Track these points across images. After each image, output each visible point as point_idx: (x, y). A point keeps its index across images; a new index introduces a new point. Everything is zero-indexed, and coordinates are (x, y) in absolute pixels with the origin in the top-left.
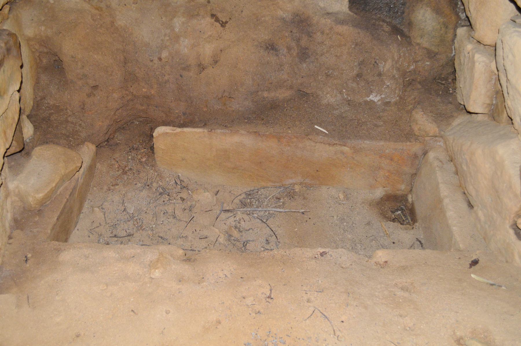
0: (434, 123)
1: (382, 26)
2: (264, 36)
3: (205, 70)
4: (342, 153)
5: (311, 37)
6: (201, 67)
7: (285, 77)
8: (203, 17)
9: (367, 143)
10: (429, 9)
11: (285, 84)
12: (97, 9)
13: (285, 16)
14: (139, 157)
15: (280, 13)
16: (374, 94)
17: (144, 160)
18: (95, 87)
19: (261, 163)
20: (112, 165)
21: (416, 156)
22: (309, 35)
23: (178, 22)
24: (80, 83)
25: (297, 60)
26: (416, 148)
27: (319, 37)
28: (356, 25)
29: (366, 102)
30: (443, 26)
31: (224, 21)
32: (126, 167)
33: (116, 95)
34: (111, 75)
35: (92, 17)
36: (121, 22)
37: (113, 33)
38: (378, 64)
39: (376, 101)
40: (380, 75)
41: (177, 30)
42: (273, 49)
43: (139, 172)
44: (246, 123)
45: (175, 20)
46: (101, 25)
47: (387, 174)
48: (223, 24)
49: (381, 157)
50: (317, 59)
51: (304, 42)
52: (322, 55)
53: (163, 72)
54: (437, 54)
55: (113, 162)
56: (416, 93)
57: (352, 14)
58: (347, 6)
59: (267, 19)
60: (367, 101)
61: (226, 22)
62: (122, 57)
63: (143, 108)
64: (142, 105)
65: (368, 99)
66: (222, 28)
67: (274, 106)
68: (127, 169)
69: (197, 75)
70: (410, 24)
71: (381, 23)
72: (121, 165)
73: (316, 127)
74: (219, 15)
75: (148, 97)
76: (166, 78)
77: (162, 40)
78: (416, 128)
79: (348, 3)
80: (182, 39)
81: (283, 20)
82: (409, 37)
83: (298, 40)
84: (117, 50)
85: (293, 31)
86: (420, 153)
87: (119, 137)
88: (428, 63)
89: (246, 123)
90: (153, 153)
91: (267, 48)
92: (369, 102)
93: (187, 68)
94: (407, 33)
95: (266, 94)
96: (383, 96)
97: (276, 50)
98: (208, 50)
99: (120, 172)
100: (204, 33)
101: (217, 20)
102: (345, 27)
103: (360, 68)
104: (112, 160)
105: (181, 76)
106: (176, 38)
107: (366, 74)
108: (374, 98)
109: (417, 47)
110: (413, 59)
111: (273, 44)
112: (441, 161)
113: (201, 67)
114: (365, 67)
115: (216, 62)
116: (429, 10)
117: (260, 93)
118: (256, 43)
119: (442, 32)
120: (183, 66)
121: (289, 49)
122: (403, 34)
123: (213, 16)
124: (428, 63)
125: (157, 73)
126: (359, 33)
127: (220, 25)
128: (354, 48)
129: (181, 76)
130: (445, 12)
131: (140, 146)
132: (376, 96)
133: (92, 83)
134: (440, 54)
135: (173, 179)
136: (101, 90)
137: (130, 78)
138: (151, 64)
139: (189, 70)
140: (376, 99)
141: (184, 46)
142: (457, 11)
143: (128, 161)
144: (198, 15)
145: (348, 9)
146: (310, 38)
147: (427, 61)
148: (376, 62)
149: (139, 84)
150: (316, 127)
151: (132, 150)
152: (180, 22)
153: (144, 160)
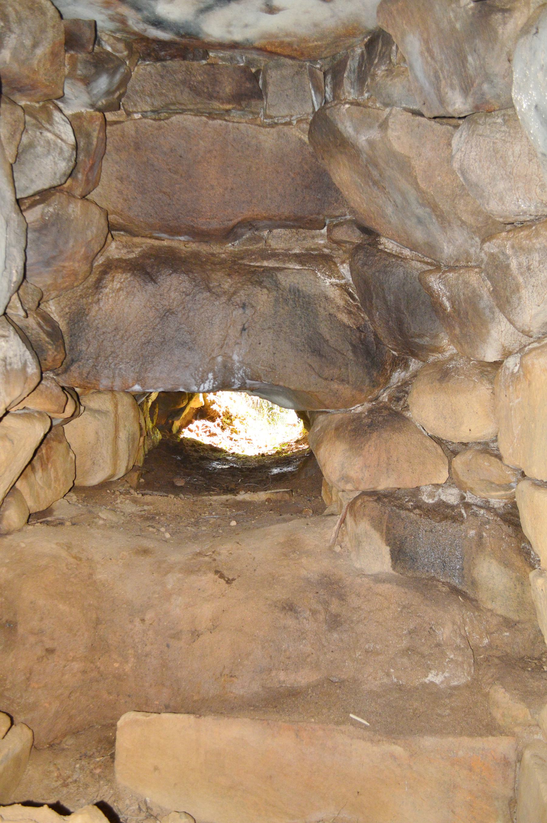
0: (522, 703)
1: (436, 586)
2: (280, 594)
3: (201, 636)
4: (393, 757)
5: (343, 600)
6: (196, 634)
7: (309, 649)
8: (205, 573)
9: (429, 742)
10: (493, 561)
11: (308, 660)
12: (76, 558)
13: (309, 576)
14: (92, 767)
15: (304, 573)
16: (433, 672)
17: (98, 771)
18: (50, 651)
19: (271, 777)
20: (50, 772)
21: (506, 762)
22: (342, 597)
23: (171, 580)
24: (32, 639)
25: (325, 627)
26: (502, 745)
27: (354, 601)
28: (399, 583)
29: (424, 685)
30: (517, 583)
31: (231, 578)
32: (69, 777)
33: (76, 666)
34: (75, 635)
35: (67, 565)
36: (101, 576)
37: (88, 586)
38: (434, 631)
39: (437, 682)
40: (438, 645)
41: (169, 587)
42: (291, 610)
43: (86, 786)
44: (251, 710)
45: (169, 575)
46: (76, 575)
47: (468, 798)
48: (229, 582)
49: (453, 765)
50: (352, 628)
51: (335, 607)
52: (358, 622)
53: (144, 639)
54: (518, 622)
55: (52, 768)
56: (493, 670)
57: (397, 574)
58: (390, 564)
59: (286, 578)
60: (425, 683)
61: (233, 580)
62: (94, 616)
63: (111, 697)
64: (110, 693)
65: (426, 680)
66: (227, 585)
67: (294, 693)
68: (70, 780)
69: (190, 645)
70: (474, 583)
71: (435, 582)
72: (63, 774)
73: (351, 715)
74: (226, 573)
75: (119, 678)
76: (147, 649)
77: (149, 598)
78: (497, 714)
79: (390, 560)
80: (175, 596)
81: (308, 581)
82: (476, 601)
83: (326, 603)
84: (90, 605)
85: (320, 593)
86: (512, 757)
87: (69, 742)
88: (507, 634)
89: (251, 710)
90: (113, 762)
91: (284, 608)
92: (429, 684)
93: (176, 636)
94: (472, 596)
95: (282, 676)
96: (447, 675)
97: (296, 612)
98: (206, 611)
99: (59, 783)
100: (203, 591)
101: (222, 576)
102: (388, 586)
103: (411, 637)
104: (51, 765)
105: (168, 646)
106: (167, 596)
107: (421, 649)
108: (435, 678)
109: (489, 614)
110: (485, 628)
111: (291, 604)
112: (540, 758)
113: (196, 634)
114: (417, 635)
115: (215, 627)
116: (494, 563)
117: (274, 673)
118: (268, 602)
119: (517, 590)
120: (172, 632)
121: (314, 612)
122: (464, 595)
123: (217, 572)
124: (507, 634)
125: (137, 640)
126: (406, 593)
127: (225, 582)
128: (401, 611)
129: (168, 646)
130: (516, 563)
131: (97, 754)
132: (437, 675)
133: (49, 644)
134: (522, 623)
135: (136, 803)
136: (59, 656)
137: (98, 647)
138: (130, 626)
139: (179, 639)
140: (438, 680)
141: (177, 608)
142: (530, 562)
143: (74, 770)
144: (199, 570)
145: (391, 569)
146: (342, 602)
147: (506, 632)
148: (431, 628)
149: (110, 656)
150: (351, 715)
151: (83, 758)
152: (175, 578)
153: (98, 771)
